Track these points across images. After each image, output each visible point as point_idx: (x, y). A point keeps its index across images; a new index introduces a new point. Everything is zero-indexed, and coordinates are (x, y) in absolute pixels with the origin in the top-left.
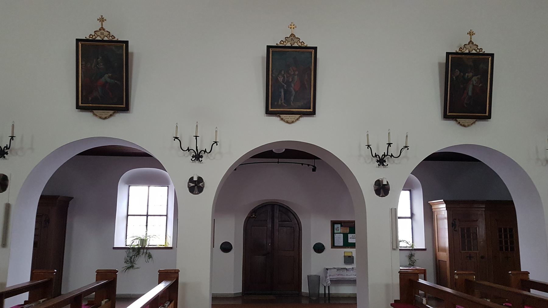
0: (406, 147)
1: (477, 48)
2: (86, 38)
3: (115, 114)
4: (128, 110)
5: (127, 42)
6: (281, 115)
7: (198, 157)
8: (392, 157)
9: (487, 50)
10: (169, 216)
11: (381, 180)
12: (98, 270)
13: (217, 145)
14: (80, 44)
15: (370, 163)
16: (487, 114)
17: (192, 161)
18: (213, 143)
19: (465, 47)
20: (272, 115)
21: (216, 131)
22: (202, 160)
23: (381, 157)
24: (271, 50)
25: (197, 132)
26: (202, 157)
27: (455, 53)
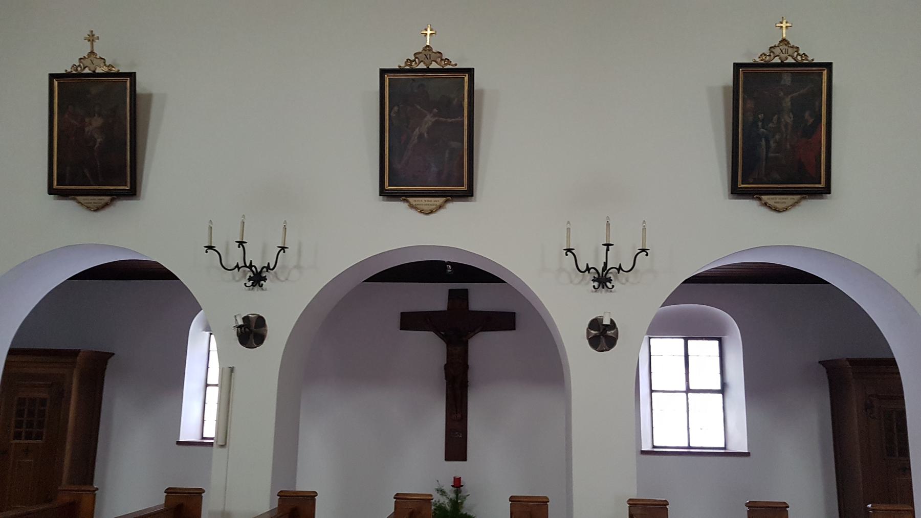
0: (643, 250)
1: (796, 53)
2: (66, 71)
3: (115, 202)
4: (472, 196)
5: (470, 71)
6: (408, 199)
7: (602, 280)
8: (621, 271)
9: (819, 58)
10: (648, 391)
11: (250, 316)
12: (281, 491)
13: (647, 255)
14: (56, 83)
15: (580, 283)
16: (822, 185)
17: (594, 289)
18: (637, 252)
19: (416, 58)
20: (393, 199)
21: (569, 229)
22: (613, 286)
23: (600, 271)
24: (387, 77)
25: (608, 236)
26: (265, 279)
27: (63, 74)
